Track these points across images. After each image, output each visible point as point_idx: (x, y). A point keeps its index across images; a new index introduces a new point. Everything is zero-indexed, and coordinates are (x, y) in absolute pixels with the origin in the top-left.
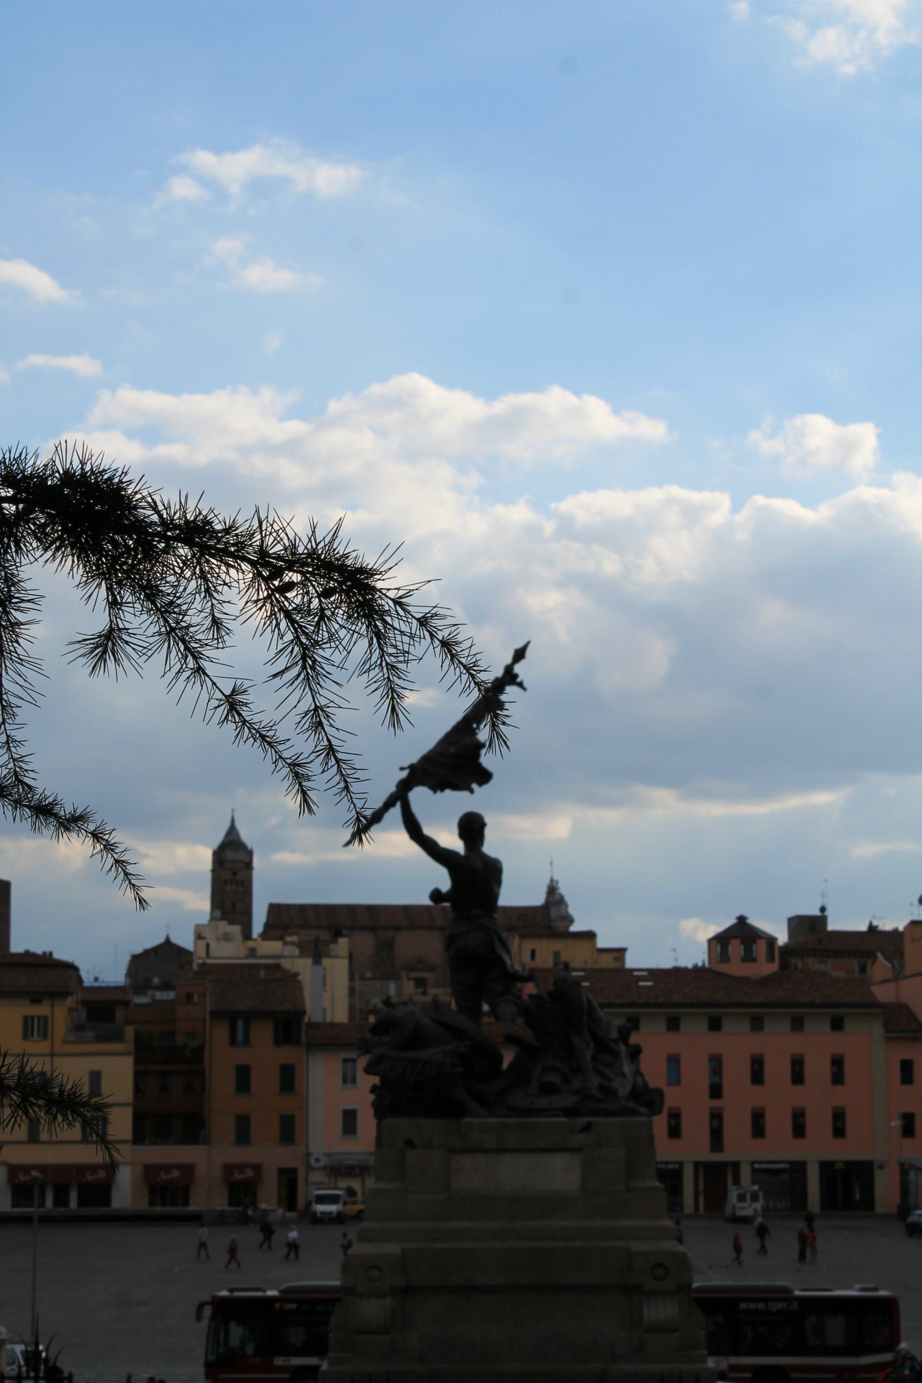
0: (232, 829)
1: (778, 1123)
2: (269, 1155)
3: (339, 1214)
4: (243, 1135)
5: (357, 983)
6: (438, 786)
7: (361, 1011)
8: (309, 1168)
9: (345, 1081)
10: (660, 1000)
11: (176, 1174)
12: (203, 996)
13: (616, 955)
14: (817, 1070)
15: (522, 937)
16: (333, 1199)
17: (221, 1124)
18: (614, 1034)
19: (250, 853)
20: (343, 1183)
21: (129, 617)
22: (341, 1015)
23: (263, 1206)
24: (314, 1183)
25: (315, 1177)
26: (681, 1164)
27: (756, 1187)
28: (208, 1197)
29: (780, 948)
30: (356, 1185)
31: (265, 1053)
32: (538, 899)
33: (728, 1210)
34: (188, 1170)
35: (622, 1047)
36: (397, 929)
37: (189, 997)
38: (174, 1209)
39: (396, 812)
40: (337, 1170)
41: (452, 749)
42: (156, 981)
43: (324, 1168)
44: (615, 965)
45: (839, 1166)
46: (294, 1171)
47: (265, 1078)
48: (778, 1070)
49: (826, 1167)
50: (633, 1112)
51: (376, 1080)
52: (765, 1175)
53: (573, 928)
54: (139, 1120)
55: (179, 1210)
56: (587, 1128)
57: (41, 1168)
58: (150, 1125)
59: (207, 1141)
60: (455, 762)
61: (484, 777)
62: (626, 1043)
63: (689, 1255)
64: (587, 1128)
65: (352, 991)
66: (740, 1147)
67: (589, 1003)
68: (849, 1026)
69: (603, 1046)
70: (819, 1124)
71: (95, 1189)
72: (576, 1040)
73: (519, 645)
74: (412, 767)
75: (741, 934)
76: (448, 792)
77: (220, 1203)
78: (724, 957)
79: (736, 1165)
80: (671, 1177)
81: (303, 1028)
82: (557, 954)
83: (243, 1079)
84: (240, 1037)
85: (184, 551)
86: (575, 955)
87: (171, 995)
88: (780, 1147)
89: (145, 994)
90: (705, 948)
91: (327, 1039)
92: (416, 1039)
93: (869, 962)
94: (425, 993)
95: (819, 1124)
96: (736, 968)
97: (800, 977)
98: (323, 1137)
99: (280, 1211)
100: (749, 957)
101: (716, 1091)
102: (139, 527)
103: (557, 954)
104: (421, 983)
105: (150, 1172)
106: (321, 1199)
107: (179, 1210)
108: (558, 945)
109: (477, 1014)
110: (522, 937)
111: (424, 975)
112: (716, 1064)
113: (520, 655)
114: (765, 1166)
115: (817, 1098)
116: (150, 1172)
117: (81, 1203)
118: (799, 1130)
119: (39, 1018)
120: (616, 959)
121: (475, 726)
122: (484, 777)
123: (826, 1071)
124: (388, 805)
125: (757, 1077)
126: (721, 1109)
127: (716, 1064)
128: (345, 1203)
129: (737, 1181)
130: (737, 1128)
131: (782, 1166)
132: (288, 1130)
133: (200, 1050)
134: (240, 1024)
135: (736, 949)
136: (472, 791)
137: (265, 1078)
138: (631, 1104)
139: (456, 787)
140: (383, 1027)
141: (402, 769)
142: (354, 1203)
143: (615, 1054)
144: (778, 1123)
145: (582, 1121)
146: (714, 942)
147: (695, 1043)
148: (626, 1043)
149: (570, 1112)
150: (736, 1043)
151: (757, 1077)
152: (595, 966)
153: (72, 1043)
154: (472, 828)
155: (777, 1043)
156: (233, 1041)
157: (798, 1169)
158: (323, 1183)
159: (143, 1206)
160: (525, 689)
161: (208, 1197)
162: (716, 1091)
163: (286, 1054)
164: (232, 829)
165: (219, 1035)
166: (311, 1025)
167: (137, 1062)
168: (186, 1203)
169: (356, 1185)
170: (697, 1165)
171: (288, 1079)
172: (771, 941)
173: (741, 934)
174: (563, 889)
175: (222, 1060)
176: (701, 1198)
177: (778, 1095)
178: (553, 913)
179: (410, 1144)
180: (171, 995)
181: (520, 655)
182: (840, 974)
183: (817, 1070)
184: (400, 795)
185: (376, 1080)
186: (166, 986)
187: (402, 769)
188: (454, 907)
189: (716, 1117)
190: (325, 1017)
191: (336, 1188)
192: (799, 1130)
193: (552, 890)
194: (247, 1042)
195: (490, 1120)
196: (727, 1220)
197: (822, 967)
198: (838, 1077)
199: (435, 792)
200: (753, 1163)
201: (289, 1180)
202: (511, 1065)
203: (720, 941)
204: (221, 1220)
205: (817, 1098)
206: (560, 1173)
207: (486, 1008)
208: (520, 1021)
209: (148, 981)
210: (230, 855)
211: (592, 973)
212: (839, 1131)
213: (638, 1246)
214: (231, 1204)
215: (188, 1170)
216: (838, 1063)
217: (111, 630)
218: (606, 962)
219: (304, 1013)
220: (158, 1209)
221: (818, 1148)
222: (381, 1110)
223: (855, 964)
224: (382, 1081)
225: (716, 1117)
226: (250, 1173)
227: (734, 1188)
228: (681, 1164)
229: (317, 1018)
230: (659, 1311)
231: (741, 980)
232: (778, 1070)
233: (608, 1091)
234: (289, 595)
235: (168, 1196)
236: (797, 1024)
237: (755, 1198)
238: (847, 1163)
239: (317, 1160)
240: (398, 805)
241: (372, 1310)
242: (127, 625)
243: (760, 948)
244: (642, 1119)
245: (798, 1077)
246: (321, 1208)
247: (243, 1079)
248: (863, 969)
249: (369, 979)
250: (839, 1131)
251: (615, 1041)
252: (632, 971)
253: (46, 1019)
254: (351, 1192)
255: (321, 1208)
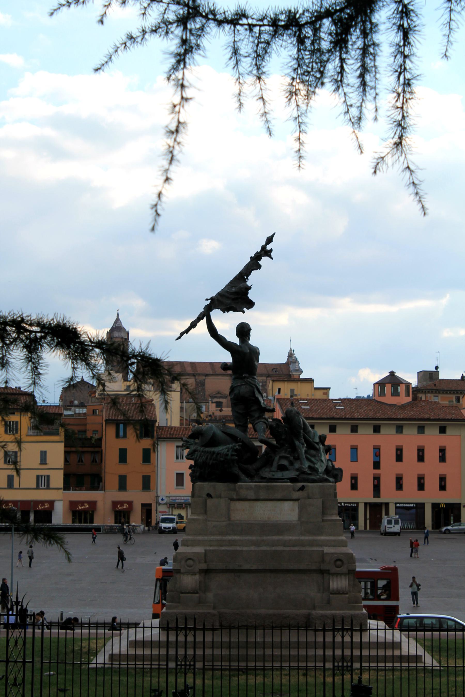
0: (118, 319)
1: (410, 483)
2: (136, 496)
3: (174, 528)
4: (123, 486)
5: (185, 404)
6: (226, 309)
7: (186, 420)
8: (158, 504)
9: (177, 458)
10: (347, 416)
11: (87, 506)
12: (102, 411)
13: (325, 391)
14: (432, 455)
15: (273, 381)
16: (171, 521)
17: (111, 480)
18: (317, 440)
19: (128, 333)
20: (176, 512)
21: (78, 373)
22: (176, 423)
23: (133, 524)
24: (160, 512)
25: (161, 508)
26: (357, 504)
27: (398, 517)
28: (104, 518)
29: (413, 388)
30: (183, 513)
31: (134, 445)
32: (283, 360)
33: (382, 529)
34: (93, 504)
35: (321, 447)
36: (207, 375)
37: (94, 412)
38: (86, 524)
39: (203, 323)
40: (173, 505)
41: (233, 290)
42: (76, 402)
43: (166, 504)
44: (324, 397)
45: (443, 505)
46: (150, 505)
47: (135, 456)
48: (410, 454)
49: (435, 506)
50: (326, 481)
51: (192, 462)
52: (402, 510)
53: (302, 377)
54: (67, 476)
55: (88, 525)
56: (302, 488)
57: (15, 503)
58: (72, 480)
59: (103, 489)
60: (235, 296)
61: (250, 304)
62: (323, 445)
63: (354, 555)
64: (302, 488)
65: (182, 409)
66: (389, 495)
67: (304, 423)
68: (448, 431)
69: (311, 446)
70: (432, 483)
71: (45, 514)
72: (297, 443)
73: (269, 235)
74: (212, 299)
75: (392, 380)
76: (231, 312)
77: (110, 522)
78: (382, 394)
79: (387, 505)
80: (349, 513)
81: (155, 429)
82: (292, 391)
83: (123, 456)
84: (121, 434)
85: (97, 350)
86: (302, 392)
87: (85, 410)
88: (410, 495)
89: (70, 410)
90: (372, 387)
91: (169, 435)
92: (213, 441)
93: (461, 396)
94: (221, 411)
95: (432, 483)
96: (389, 399)
97: (424, 404)
98: (166, 487)
99: (142, 527)
100: (396, 393)
101: (377, 465)
102: (82, 343)
103: (292, 391)
104: (219, 405)
105: (73, 504)
106: (164, 521)
107: (88, 525)
108: (292, 386)
109: (244, 428)
110: (273, 381)
111: (221, 400)
112: (377, 451)
113: (270, 240)
114: (402, 505)
115: (432, 469)
116: (73, 504)
117: (36, 521)
118: (421, 486)
119: (13, 422)
120: (324, 394)
121: (246, 277)
122: (250, 304)
123: (437, 454)
124: (199, 319)
125: (399, 458)
126: (380, 474)
127: (377, 451)
128: (177, 523)
129: (387, 513)
130: (387, 484)
131: (412, 505)
132: (147, 483)
133: (100, 440)
134: (121, 426)
135: (389, 389)
136: (244, 312)
137: (135, 456)
138: (325, 476)
139: (235, 310)
140: (196, 435)
141: (207, 300)
142: (181, 522)
143: (318, 450)
144: (410, 483)
145: (300, 485)
146: (377, 385)
147: (366, 439)
148: (323, 445)
149: (293, 480)
150: (388, 439)
151: (399, 458)
152: (313, 398)
153: (31, 435)
154: (243, 331)
155: (410, 440)
156: (117, 436)
157: (420, 507)
158: (165, 512)
159: (69, 523)
160: (272, 259)
161: (104, 518)
162: (377, 465)
163: (146, 443)
164: (118, 319)
165: (110, 432)
166: (160, 428)
167: (65, 447)
168: (92, 522)
169: (183, 513)
170: (366, 504)
171: (147, 456)
172: (408, 385)
173: (392, 380)
174: (297, 355)
175: (111, 445)
176: (368, 522)
177: (410, 469)
178: (292, 367)
179: (209, 496)
180: (85, 410)
181: (270, 240)
182: (446, 403)
183: (432, 455)
184: (206, 314)
185: (192, 462)
186: (82, 405)
187: (207, 300)
188: (234, 373)
189: (377, 479)
190: (167, 423)
191: (172, 515)
192: (421, 486)
193: (291, 355)
194: (125, 436)
195: (251, 484)
196: (382, 534)
197: (436, 399)
198: (443, 459)
199: (224, 312)
200: (396, 504)
201: (147, 510)
202: (266, 451)
203: (381, 384)
204: (110, 531)
205: (432, 469)
206: (287, 512)
207: (250, 426)
208: (268, 432)
209: (72, 402)
210: (116, 334)
211: (310, 401)
212: (443, 487)
213: (326, 550)
214: (116, 523)
215: (93, 504)
216: (442, 451)
217: (72, 377)
218: (319, 395)
219: (156, 421)
220: (77, 525)
221: (431, 496)
222: (194, 478)
223: (454, 397)
224: (195, 463)
225: (377, 479)
226: (126, 506)
227: (386, 517)
228: (357, 504)
229: (163, 424)
230: (339, 583)
231: (391, 405)
232: (410, 454)
233: (313, 470)
234: (133, 366)
235: (82, 517)
236: (421, 429)
237: (396, 522)
238: (446, 504)
239: (162, 500)
240: (205, 318)
241: (189, 581)
242: (78, 375)
243: (402, 389)
244: (331, 484)
245: (421, 458)
246: (164, 525)
247: (123, 456)
248: (458, 400)
249: (191, 403)
250: (443, 487)
251: (317, 443)
252: (332, 400)
253: (17, 423)
254: (180, 517)
255: (164, 525)
